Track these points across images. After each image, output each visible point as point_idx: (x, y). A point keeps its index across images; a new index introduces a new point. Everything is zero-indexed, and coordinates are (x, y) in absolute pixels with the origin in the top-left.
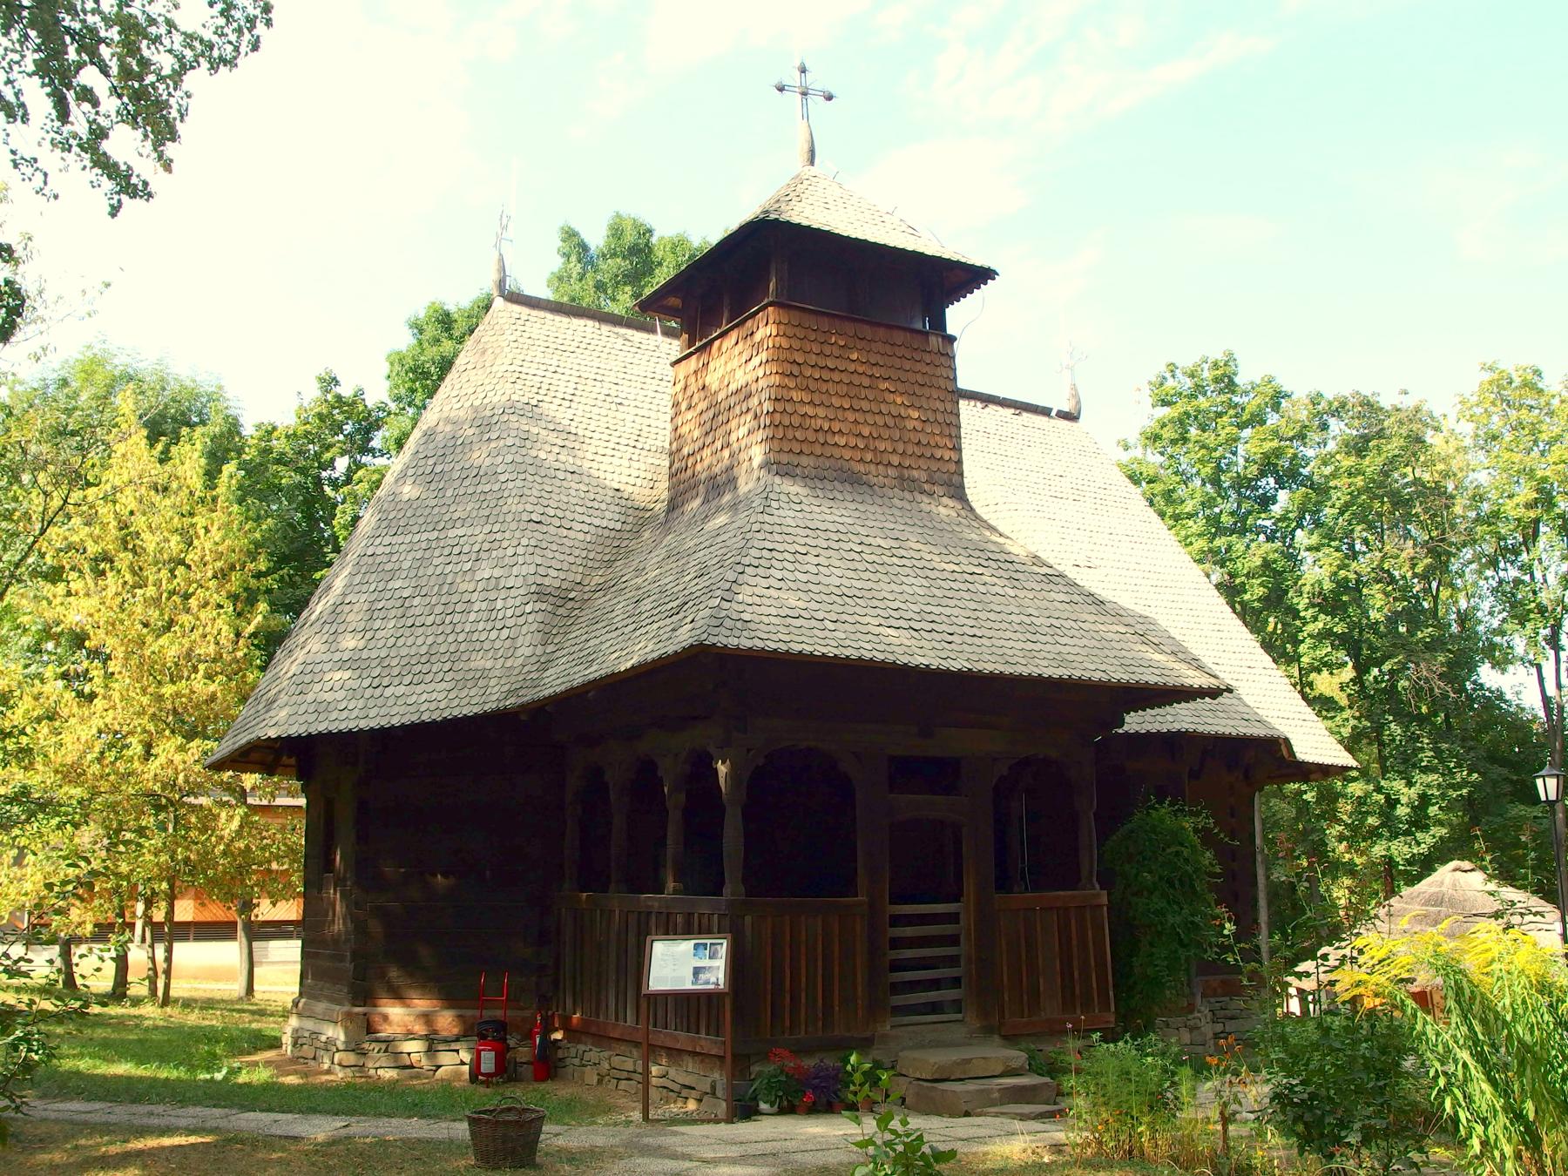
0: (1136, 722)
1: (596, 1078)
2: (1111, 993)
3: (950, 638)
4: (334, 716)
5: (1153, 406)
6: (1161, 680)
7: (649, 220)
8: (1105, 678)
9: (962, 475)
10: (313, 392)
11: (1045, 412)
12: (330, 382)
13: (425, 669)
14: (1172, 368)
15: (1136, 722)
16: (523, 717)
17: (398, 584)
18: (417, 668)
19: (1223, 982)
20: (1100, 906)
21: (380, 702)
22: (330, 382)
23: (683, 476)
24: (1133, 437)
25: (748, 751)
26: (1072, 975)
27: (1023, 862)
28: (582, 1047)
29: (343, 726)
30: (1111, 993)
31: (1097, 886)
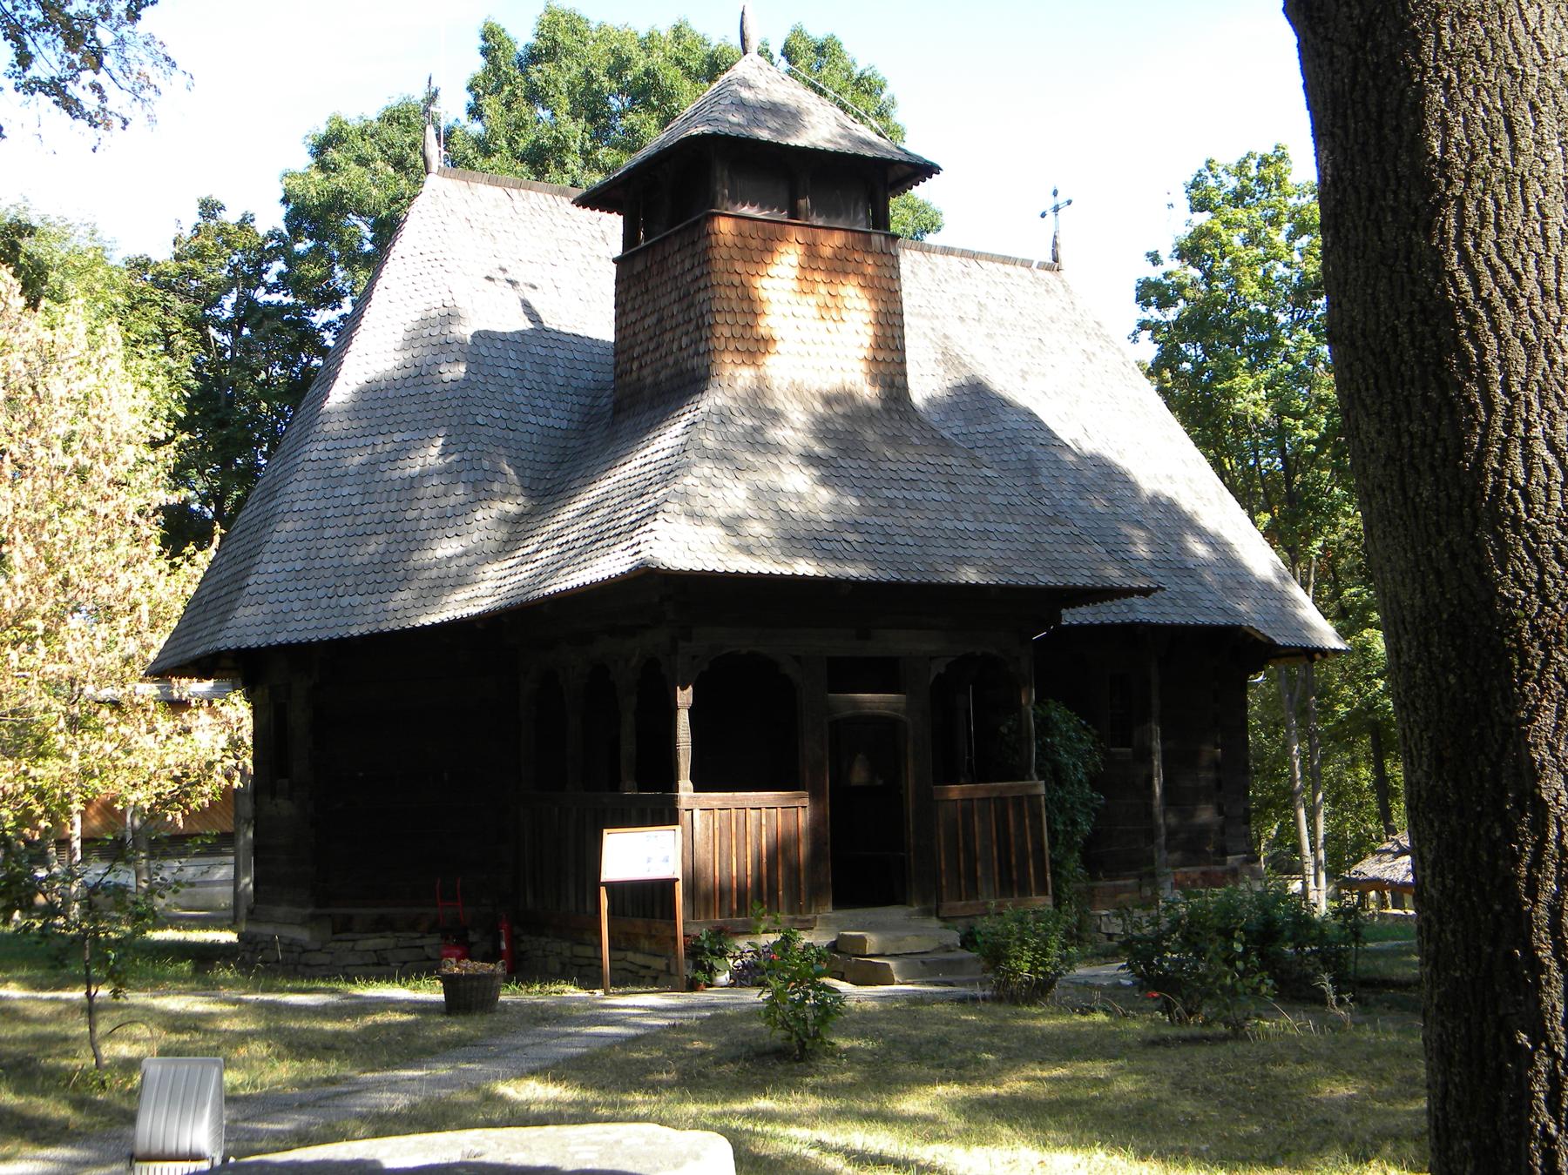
0: (1072, 617)
1: (558, 967)
2: (1049, 878)
3: (882, 549)
4: (291, 627)
5: (1192, 210)
6: (1090, 583)
7: (584, 12)
8: (1032, 582)
9: (905, 375)
10: (192, 217)
11: (1027, 264)
12: (209, 208)
13: (379, 578)
14: (1209, 165)
15: (1071, 617)
16: (479, 626)
17: (345, 491)
18: (371, 578)
19: (1204, 873)
20: (1039, 796)
21: (336, 612)
22: (209, 208)
23: (628, 379)
24: (1166, 251)
25: (694, 657)
26: (1009, 861)
27: (970, 754)
28: (543, 940)
29: (303, 637)
30: (1049, 878)
31: (1035, 777)
